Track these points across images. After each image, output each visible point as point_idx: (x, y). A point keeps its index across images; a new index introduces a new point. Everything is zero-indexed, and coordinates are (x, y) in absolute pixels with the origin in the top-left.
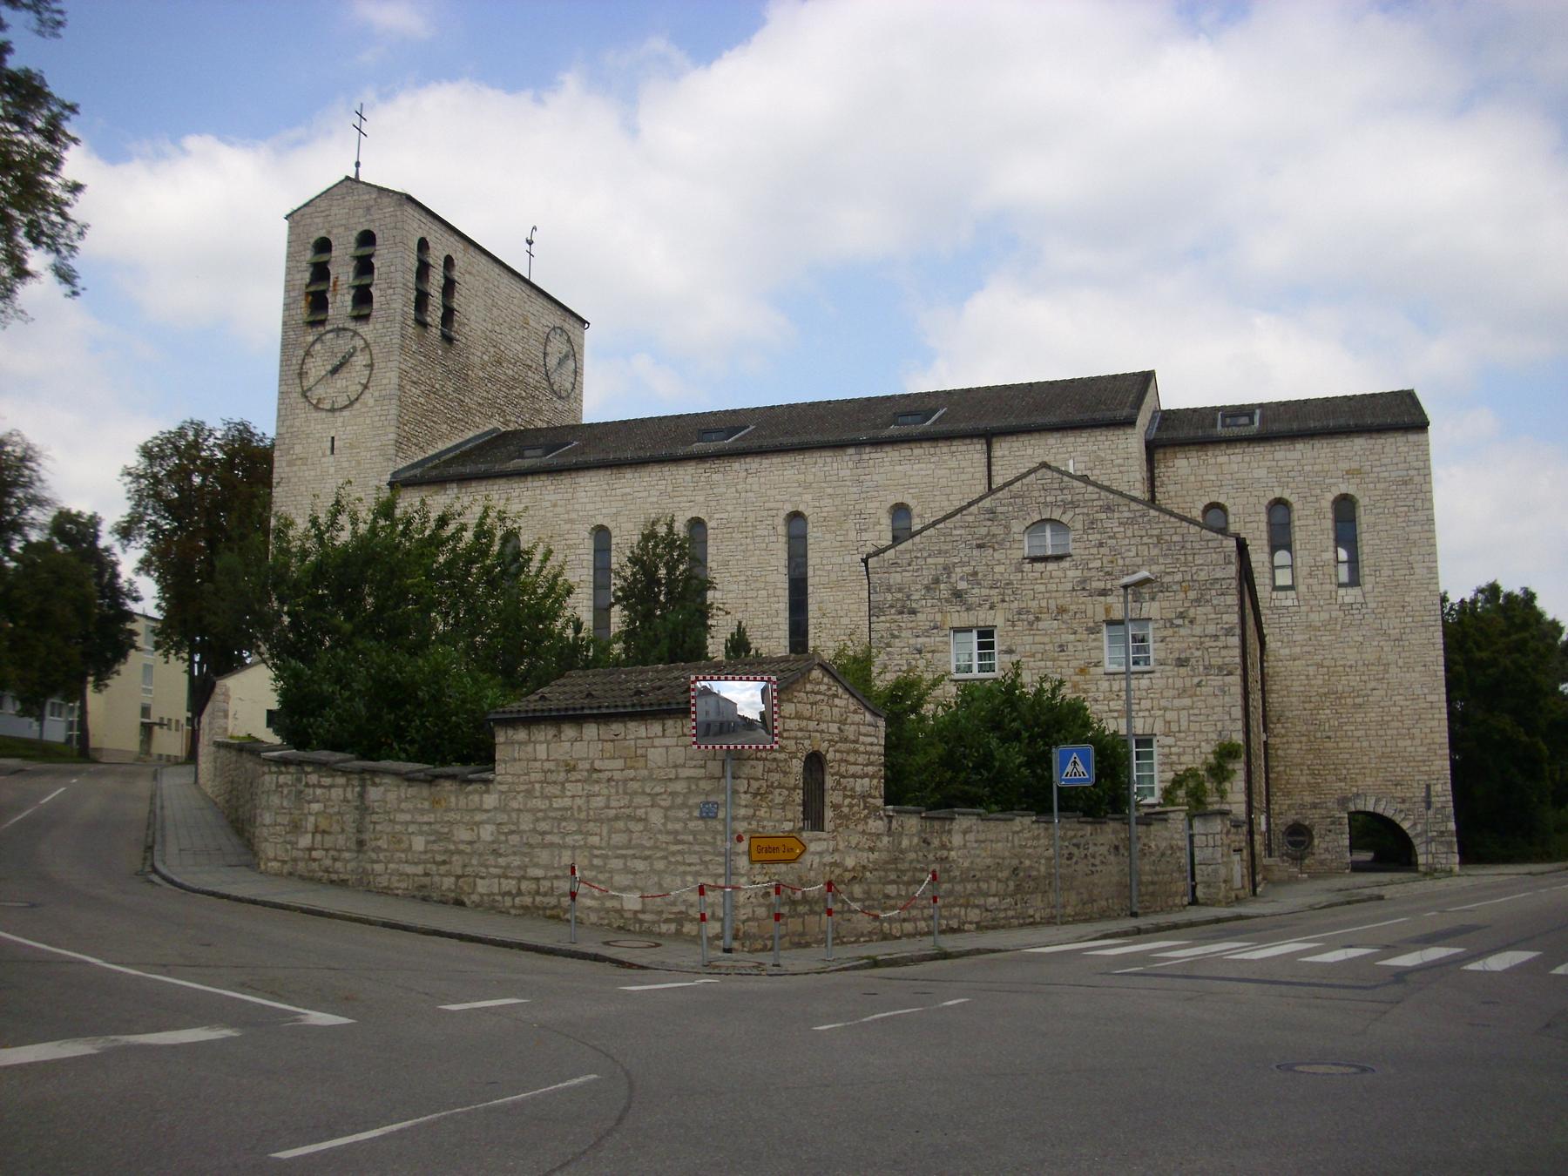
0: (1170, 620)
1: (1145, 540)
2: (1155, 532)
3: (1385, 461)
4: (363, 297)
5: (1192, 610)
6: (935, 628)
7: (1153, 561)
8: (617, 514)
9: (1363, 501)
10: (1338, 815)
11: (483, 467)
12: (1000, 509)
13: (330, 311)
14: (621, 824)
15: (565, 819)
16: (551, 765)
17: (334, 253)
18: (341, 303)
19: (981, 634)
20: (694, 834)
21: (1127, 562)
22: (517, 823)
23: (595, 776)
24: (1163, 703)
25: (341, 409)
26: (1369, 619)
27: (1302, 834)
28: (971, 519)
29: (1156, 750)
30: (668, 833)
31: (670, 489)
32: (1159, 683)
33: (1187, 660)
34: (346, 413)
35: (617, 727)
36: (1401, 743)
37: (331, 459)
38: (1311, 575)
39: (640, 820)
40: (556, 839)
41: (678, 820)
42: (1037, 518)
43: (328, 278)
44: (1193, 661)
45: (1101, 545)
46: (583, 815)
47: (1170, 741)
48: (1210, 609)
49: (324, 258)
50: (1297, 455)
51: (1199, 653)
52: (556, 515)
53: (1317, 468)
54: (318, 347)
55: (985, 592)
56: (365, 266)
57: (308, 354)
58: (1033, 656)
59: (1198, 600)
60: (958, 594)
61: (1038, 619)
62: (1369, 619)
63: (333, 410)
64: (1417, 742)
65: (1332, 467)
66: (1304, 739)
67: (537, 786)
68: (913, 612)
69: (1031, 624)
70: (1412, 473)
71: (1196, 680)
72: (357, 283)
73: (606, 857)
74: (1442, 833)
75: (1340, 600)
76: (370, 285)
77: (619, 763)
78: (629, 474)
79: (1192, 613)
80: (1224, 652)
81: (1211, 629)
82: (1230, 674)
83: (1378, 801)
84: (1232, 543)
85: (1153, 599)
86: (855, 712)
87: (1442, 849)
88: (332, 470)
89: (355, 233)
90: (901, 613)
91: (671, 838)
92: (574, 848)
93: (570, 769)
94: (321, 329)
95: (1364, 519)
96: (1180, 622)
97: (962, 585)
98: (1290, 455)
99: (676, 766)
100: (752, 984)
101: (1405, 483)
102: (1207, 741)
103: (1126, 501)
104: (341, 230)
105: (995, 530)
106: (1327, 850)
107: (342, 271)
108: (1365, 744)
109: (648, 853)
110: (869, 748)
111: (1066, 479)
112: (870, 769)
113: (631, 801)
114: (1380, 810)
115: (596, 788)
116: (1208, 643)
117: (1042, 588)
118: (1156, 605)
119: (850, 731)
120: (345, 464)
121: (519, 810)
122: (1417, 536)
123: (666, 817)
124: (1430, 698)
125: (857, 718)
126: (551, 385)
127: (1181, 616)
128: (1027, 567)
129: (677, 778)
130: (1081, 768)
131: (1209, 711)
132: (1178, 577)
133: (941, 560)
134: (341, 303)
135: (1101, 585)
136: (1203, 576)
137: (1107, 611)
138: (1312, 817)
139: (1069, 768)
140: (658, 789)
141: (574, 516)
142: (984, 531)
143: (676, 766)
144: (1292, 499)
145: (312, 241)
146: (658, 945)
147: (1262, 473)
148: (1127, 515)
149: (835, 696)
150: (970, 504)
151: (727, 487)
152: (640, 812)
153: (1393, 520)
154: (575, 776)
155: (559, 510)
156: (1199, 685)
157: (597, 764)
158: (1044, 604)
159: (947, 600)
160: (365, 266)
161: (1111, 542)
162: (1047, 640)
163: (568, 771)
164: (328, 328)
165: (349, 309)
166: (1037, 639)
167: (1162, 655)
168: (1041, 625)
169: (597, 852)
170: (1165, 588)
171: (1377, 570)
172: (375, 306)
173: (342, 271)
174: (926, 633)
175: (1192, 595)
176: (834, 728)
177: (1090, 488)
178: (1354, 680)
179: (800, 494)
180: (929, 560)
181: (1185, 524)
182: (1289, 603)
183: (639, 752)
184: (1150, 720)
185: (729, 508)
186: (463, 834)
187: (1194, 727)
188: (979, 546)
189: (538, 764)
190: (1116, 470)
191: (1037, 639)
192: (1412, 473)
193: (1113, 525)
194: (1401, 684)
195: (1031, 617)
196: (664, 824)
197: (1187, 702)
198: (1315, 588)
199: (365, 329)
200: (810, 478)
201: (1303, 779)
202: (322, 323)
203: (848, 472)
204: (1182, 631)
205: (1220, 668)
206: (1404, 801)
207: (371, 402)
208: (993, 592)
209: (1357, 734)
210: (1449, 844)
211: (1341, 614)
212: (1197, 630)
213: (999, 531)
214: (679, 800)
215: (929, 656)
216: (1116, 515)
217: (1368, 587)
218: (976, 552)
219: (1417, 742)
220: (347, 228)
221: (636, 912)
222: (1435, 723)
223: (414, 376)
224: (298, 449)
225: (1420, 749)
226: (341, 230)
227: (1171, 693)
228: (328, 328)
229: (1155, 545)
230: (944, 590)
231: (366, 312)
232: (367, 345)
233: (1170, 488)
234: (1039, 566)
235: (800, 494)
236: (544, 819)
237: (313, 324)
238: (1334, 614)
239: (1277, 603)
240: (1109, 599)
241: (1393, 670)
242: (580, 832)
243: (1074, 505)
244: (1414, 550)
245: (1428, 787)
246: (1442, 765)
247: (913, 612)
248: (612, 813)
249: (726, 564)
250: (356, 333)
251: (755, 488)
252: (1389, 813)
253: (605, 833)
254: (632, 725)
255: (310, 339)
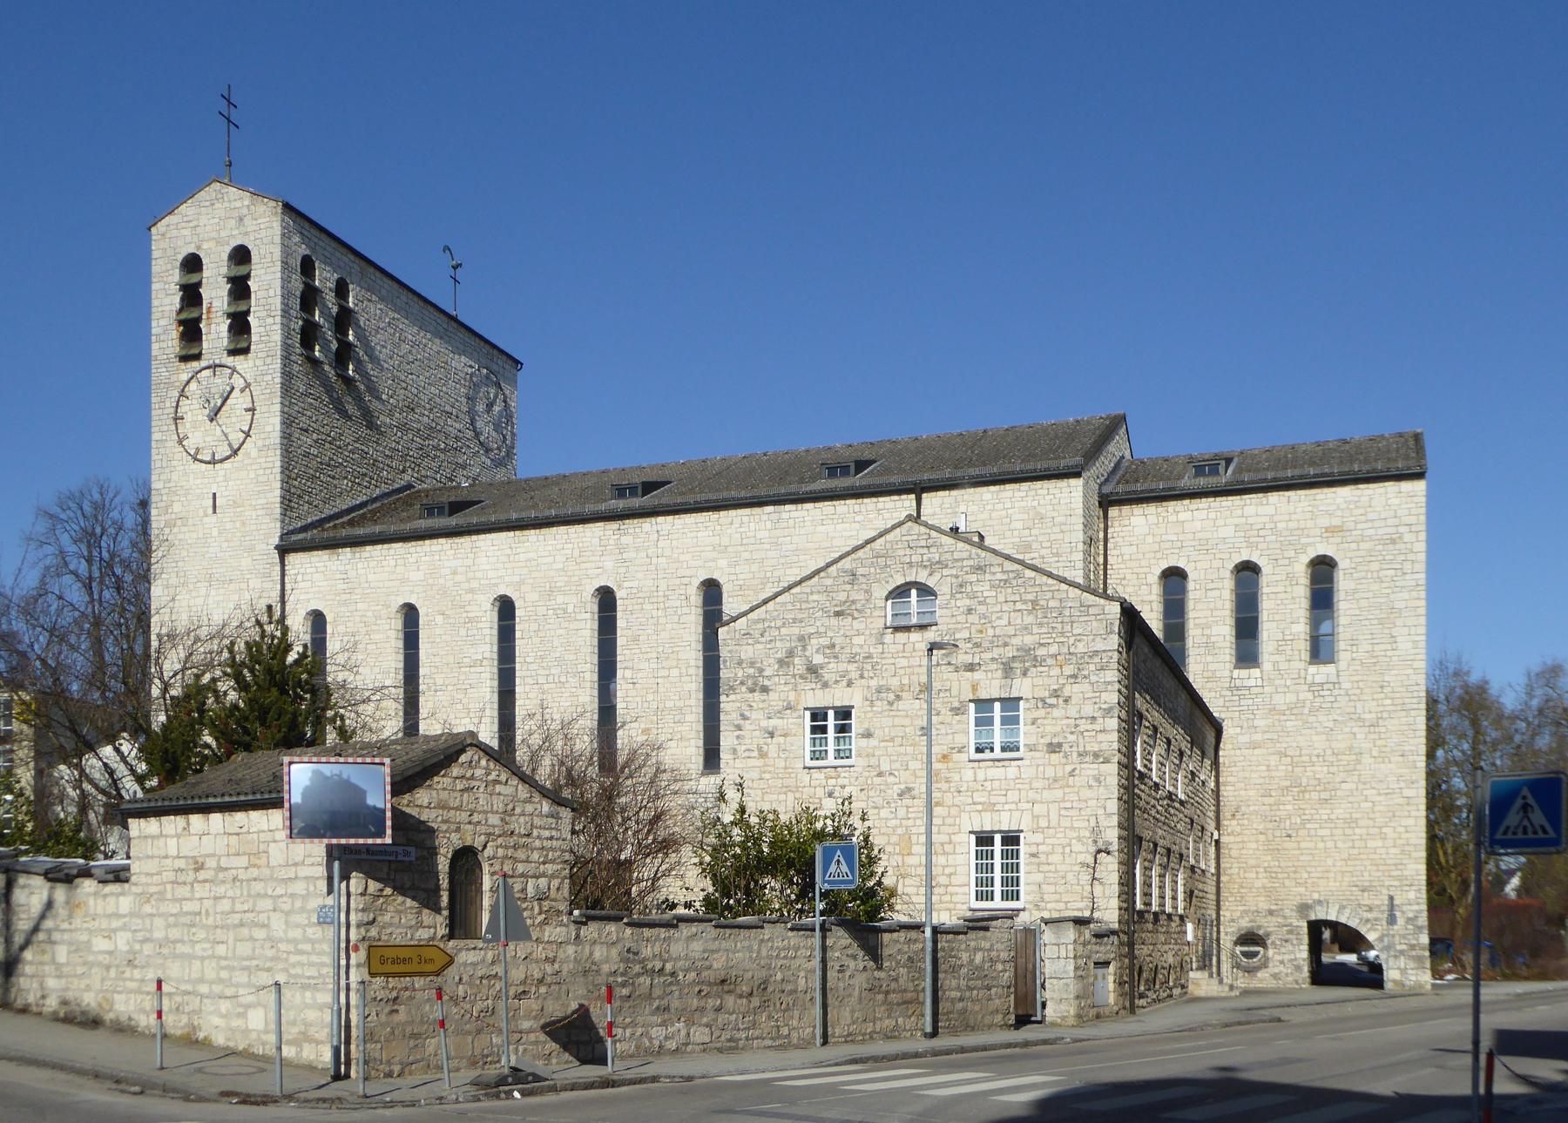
0: (1043, 700)
1: (1019, 606)
2: (1030, 597)
3: (1371, 516)
4: (240, 325)
5: (1068, 687)
6: (789, 708)
7: (1026, 629)
8: (521, 583)
9: (1343, 564)
10: (1296, 923)
11: (377, 529)
12: (861, 571)
13: (205, 345)
14: (245, 932)
15: (193, 925)
16: (181, 863)
17: (205, 273)
18: (216, 332)
19: (814, 717)
20: (312, 941)
21: (998, 632)
22: (151, 931)
23: (221, 875)
24: (1031, 794)
25: (221, 461)
26: (1343, 700)
27: (1257, 944)
28: (829, 582)
29: (1022, 848)
30: (288, 941)
31: (576, 553)
32: (1027, 773)
33: (1060, 745)
34: (227, 465)
35: (240, 816)
36: (1371, 844)
37: (214, 518)
38: (1278, 652)
39: (264, 926)
40: (186, 949)
41: (298, 926)
42: (900, 581)
43: (201, 304)
44: (1066, 747)
45: (970, 611)
46: (210, 921)
47: (1038, 838)
48: (1086, 687)
49: (194, 279)
50: (1270, 510)
51: (1072, 738)
52: (457, 584)
53: (1292, 525)
54: (193, 386)
55: (843, 666)
56: (240, 288)
57: (182, 394)
58: (892, 740)
59: (1074, 676)
60: (813, 670)
61: (898, 697)
62: (1343, 700)
63: (213, 462)
64: (1390, 843)
65: (1310, 524)
66: (1262, 838)
67: (169, 887)
68: (765, 690)
69: (891, 704)
70: (1402, 529)
71: (1069, 768)
72: (232, 310)
73: (231, 969)
74: (1412, 947)
75: (1309, 679)
76: (248, 312)
77: (243, 861)
78: (532, 534)
79: (1067, 692)
80: (1101, 737)
81: (1088, 710)
82: (1106, 761)
83: (1342, 908)
84: (1115, 609)
85: (1024, 674)
86: (529, 800)
87: (1412, 964)
88: (215, 532)
89: (228, 249)
90: (752, 691)
91: (291, 948)
92: (203, 959)
93: (199, 867)
94: (195, 365)
95: (1343, 583)
96: (1053, 701)
97: (818, 659)
98: (1261, 510)
99: (296, 864)
100: (357, 1115)
101: (1393, 542)
102: (1079, 839)
103: (1000, 560)
104: (212, 244)
105: (854, 596)
106: (1282, 962)
107: (215, 294)
108: (1330, 844)
109: (268, 964)
110: (548, 844)
111: (934, 534)
112: (550, 868)
113: (255, 905)
114: (1343, 920)
115: (221, 890)
116: (1084, 725)
117: (904, 662)
118: (1027, 682)
119: (519, 824)
120: (229, 525)
121: (152, 915)
122: (1401, 605)
123: (287, 922)
124: (1407, 793)
125: (529, 808)
126: (477, 434)
127: (1056, 694)
128: (889, 638)
129: (272, 878)
130: (844, 868)
131: (1083, 805)
132: (1054, 649)
133: (796, 631)
134: (216, 332)
135: (968, 659)
136: (1081, 648)
137: (974, 688)
138: (1267, 925)
139: (833, 868)
140: (279, 891)
141: (474, 584)
142: (842, 596)
143: (296, 864)
144: (1261, 562)
145: (180, 257)
146: (263, 1070)
147: (1228, 532)
148: (1000, 576)
149: (496, 782)
150: (828, 565)
151: (637, 550)
152: (263, 918)
153: (1375, 587)
154: (202, 875)
155: (459, 578)
156: (1072, 774)
157: (224, 863)
158: (906, 681)
159: (801, 677)
160: (240, 288)
161: (982, 609)
162: (907, 722)
163: (196, 870)
164: (204, 363)
165: (226, 342)
166: (897, 721)
167: (1032, 740)
168: (901, 705)
169: (223, 963)
170: (1037, 662)
171: (1354, 642)
172: (254, 338)
173: (215, 294)
174: (779, 713)
175: (1069, 670)
176: (494, 820)
177: (961, 545)
178: (1321, 771)
179: (714, 560)
180: (784, 631)
181: (1064, 587)
182: (1252, 682)
183: (262, 847)
184: (1016, 814)
185: (639, 575)
186: (100, 944)
187: (1066, 823)
188: (838, 614)
189: (168, 862)
190: (1056, 529)
191: (897, 721)
192: (1402, 529)
193: (984, 588)
194: (1373, 776)
195: (891, 697)
196: (285, 932)
197: (1058, 794)
198: (1283, 666)
199: (238, 361)
200: (725, 541)
201: (1258, 884)
202: (198, 357)
203: (766, 534)
204: (1056, 713)
205: (1096, 755)
206: (1370, 909)
207: (254, 453)
208: (852, 667)
209: (1321, 832)
210: (1419, 959)
211: (1310, 696)
212: (1072, 711)
213: (860, 596)
214: (298, 904)
215: (782, 739)
216: (988, 577)
217: (1343, 664)
218: (834, 621)
219: (1390, 843)
220: (218, 242)
221: (259, 1032)
222: (1411, 822)
223: (304, 422)
224: (177, 507)
225: (1393, 851)
226: (212, 244)
227: (1038, 784)
228: (204, 363)
229: (1030, 612)
230: (799, 664)
231: (244, 345)
232: (248, 385)
233: (1125, 550)
234: (901, 637)
235: (714, 560)
236: (175, 925)
237: (185, 359)
238: (1302, 696)
239: (1238, 683)
240: (977, 675)
241: (1366, 760)
242: (206, 940)
243: (942, 564)
244: (1399, 622)
245: (1391, 898)
246: (1418, 869)
247: (765, 690)
248: (236, 918)
249: (636, 639)
250: (234, 370)
251: (668, 552)
252: (1353, 923)
253: (231, 941)
254: (254, 815)
255: (185, 377)
